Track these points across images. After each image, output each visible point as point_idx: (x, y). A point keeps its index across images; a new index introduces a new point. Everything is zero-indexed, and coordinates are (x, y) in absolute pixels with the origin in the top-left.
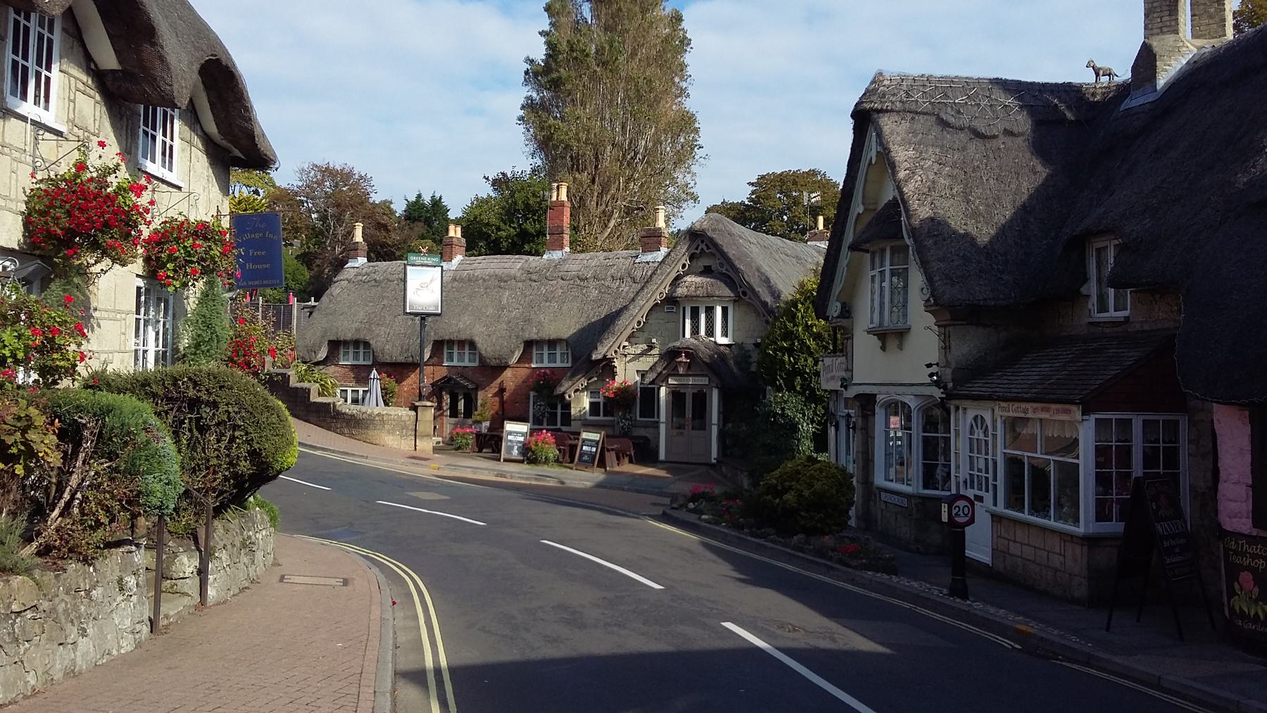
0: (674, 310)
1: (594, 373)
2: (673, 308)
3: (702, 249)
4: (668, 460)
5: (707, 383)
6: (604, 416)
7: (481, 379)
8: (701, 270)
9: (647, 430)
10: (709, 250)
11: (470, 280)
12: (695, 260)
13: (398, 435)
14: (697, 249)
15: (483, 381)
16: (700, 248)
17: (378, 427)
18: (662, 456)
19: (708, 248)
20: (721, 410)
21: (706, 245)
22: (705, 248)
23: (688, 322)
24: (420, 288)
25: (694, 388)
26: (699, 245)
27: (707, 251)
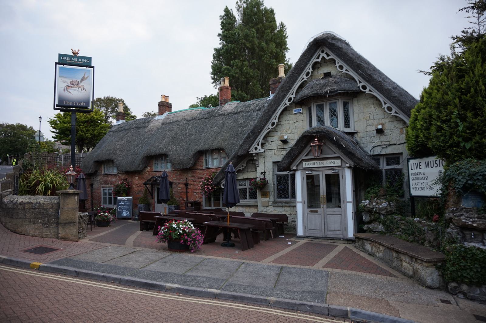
0: (301, 111)
1: (241, 166)
2: (300, 110)
3: (323, 57)
4: (307, 235)
5: (340, 165)
6: (291, 199)
7: (174, 179)
8: (322, 77)
9: (284, 208)
10: (329, 57)
11: (170, 123)
12: (316, 70)
13: (40, 223)
14: (318, 58)
15: (175, 180)
16: (321, 57)
17: (20, 216)
18: (300, 232)
19: (328, 55)
20: (354, 190)
21: (326, 54)
22: (325, 56)
23: (176, 286)
24: (70, 85)
25: (68, 261)
26: (320, 55)
27: (327, 58)
